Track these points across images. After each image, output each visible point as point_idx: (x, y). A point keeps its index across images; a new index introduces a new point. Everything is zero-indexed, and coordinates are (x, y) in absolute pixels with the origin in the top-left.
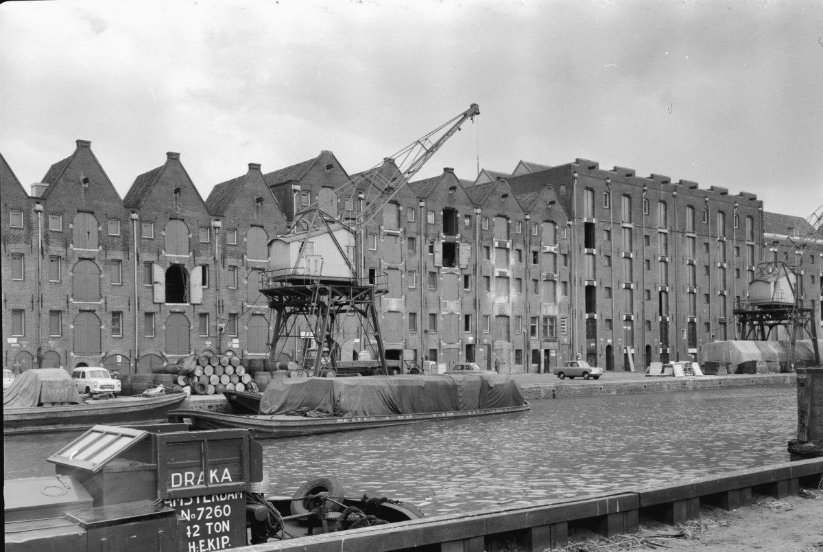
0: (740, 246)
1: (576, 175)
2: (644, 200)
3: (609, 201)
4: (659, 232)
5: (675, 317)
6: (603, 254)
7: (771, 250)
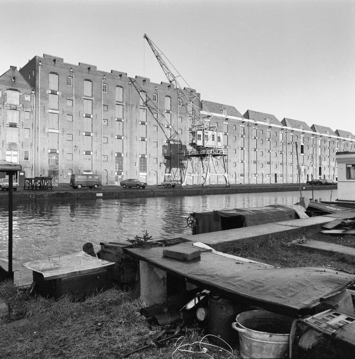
1: (40, 63)
4: (84, 99)
6: (66, 114)
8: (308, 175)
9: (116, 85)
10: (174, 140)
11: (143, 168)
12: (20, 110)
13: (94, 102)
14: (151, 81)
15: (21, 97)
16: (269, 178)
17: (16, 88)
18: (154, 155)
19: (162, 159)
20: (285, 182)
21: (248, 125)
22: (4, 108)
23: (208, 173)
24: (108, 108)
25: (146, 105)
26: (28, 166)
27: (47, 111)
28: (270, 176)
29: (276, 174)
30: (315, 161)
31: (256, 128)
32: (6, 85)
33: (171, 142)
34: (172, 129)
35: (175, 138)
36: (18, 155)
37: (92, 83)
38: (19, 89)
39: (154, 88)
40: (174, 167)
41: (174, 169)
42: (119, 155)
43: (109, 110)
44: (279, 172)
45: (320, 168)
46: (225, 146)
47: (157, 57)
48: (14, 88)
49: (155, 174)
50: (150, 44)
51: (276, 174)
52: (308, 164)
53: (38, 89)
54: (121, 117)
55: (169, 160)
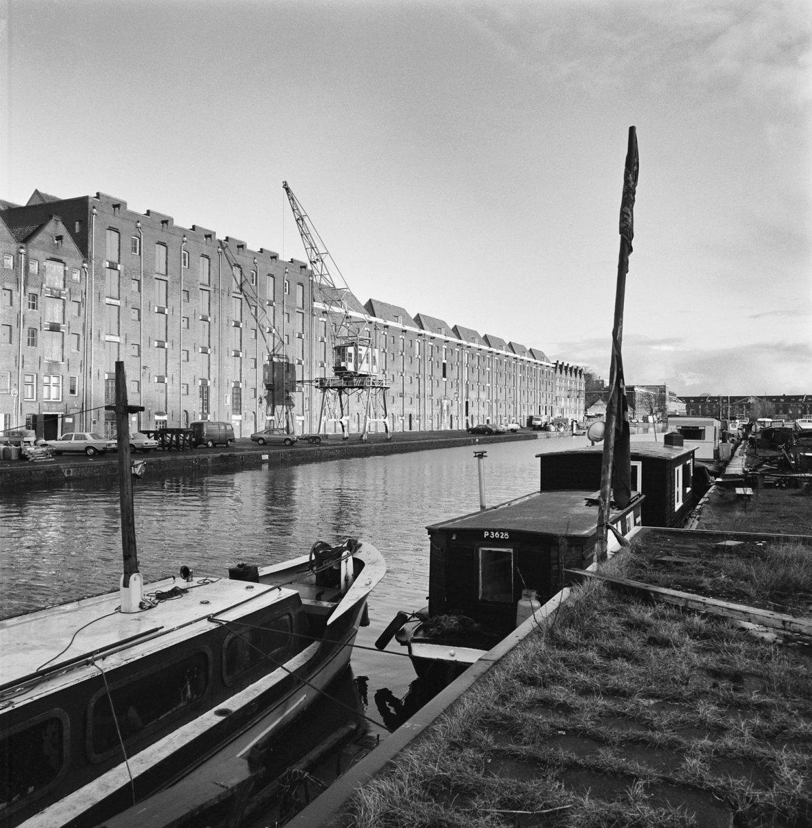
0: (290, 312)
1: (95, 210)
2: (285, 281)
3: (256, 279)
4: (201, 289)
5: (217, 381)
6: (130, 306)
7: (321, 319)
8: (451, 415)
9: (157, 240)
10: (278, 355)
11: (237, 408)
12: (65, 298)
13: (169, 285)
14: (129, 208)
15: (67, 273)
16: (401, 422)
17: (60, 258)
18: (251, 383)
19: (262, 392)
20: (422, 429)
21: (376, 327)
22: (43, 296)
23: (368, 418)
24: (188, 296)
25: (241, 290)
26: (76, 406)
27: (103, 301)
28: (403, 418)
29: (410, 415)
30: (460, 391)
31: (386, 333)
32: (45, 250)
33: (275, 359)
34: (276, 334)
35: (280, 352)
36: (60, 385)
37: (167, 249)
38: (64, 259)
39: (252, 260)
40: (279, 404)
41: (279, 408)
42: (204, 382)
43: (191, 300)
44: (415, 412)
45: (467, 403)
46: (383, 370)
47: (297, 220)
48: (57, 257)
49: (251, 417)
50: (292, 199)
51: (410, 415)
52: (452, 397)
53: (91, 257)
54: (207, 313)
55: (271, 392)
